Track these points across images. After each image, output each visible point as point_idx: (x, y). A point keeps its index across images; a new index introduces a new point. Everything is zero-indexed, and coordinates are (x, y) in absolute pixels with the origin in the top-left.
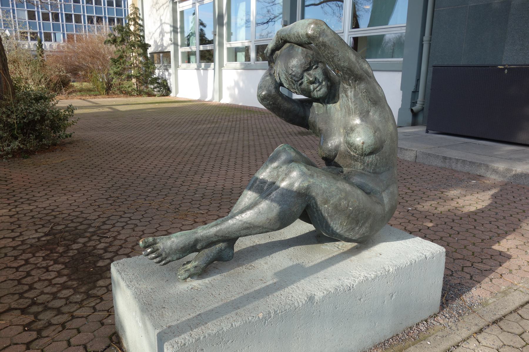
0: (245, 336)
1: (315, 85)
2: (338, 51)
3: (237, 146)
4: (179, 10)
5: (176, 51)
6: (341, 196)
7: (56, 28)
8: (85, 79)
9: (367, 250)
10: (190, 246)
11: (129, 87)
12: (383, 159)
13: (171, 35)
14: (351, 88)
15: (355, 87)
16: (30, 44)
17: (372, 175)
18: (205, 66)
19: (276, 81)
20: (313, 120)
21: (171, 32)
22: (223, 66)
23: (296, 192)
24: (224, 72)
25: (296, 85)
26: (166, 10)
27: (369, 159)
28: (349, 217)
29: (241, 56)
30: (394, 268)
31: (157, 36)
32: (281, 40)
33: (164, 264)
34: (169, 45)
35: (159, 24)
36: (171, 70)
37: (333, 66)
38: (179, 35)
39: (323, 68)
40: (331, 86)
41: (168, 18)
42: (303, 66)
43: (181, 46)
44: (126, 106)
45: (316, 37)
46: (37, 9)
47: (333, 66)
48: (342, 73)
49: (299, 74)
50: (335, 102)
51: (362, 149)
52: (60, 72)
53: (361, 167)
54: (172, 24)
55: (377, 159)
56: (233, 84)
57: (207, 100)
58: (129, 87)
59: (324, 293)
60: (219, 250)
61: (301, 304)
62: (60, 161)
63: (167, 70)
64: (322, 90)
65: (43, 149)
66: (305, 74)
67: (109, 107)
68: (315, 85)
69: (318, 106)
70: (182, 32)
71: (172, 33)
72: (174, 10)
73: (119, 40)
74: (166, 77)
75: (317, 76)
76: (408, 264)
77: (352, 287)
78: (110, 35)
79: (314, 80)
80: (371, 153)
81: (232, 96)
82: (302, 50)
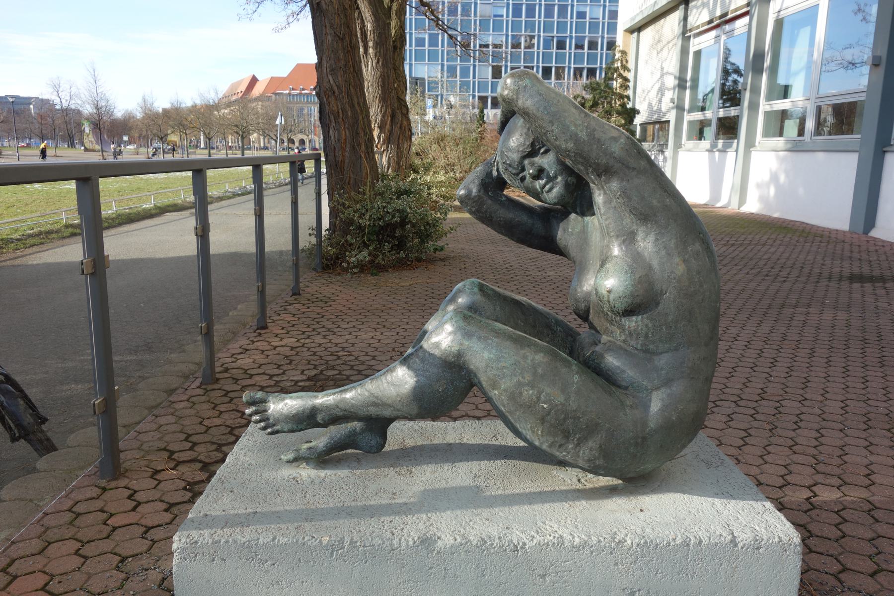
0: (294, 563)
4: (692, 49)
5: (679, 120)
6: (521, 379)
9: (628, 497)
10: (306, 414)
12: (660, 326)
13: (674, 93)
14: (599, 189)
15: (603, 188)
16: (490, 113)
17: (641, 355)
18: (723, 146)
21: (674, 88)
22: (754, 146)
23: (440, 358)
24: (755, 155)
26: (671, 52)
27: (631, 323)
28: (543, 420)
29: (791, 128)
30: (637, 540)
31: (653, 96)
33: (271, 434)
34: (669, 111)
35: (659, 76)
36: (668, 153)
38: (688, 92)
41: (672, 64)
42: (521, 149)
43: (690, 111)
46: (474, 62)
49: (516, 163)
51: (609, 302)
53: (620, 336)
54: (678, 75)
55: (647, 326)
56: (766, 177)
57: (718, 205)
59: (456, 540)
60: (350, 432)
61: (404, 544)
62: (408, 284)
64: (555, 190)
65: (402, 265)
66: (526, 162)
68: (542, 182)
70: (695, 86)
71: (677, 90)
72: (684, 51)
74: (660, 163)
76: (678, 541)
77: (522, 548)
80: (629, 312)
81: (763, 199)
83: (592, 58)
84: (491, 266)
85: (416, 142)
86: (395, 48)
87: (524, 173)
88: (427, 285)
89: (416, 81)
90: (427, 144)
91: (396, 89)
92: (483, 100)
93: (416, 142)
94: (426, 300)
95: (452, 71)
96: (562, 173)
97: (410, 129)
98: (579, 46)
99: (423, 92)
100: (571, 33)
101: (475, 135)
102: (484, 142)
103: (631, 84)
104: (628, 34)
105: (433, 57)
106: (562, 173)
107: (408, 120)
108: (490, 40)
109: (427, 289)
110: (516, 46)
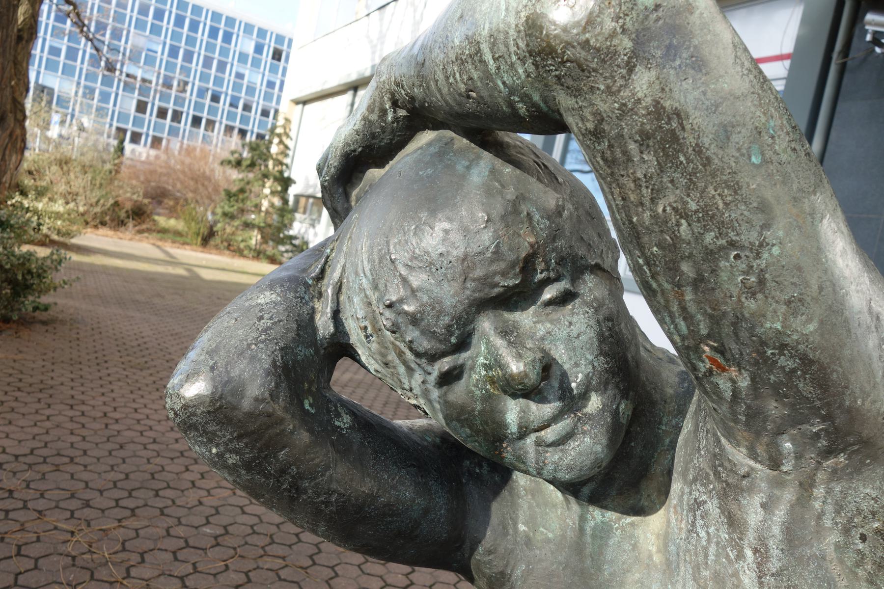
1: (533, 406)
2: (763, 207)
3: (375, 398)
7: (173, 132)
8: (172, 212)
11: (242, 241)
14: (779, 483)
15: (806, 486)
19: (306, 325)
20: (498, 565)
25: (418, 377)
32: (395, 104)
37: (688, 317)
39: (605, 311)
40: (636, 416)
42: (479, 272)
44: (217, 272)
45: (607, 55)
47: (688, 317)
48: (744, 383)
49: (446, 320)
50: (640, 511)
52: (134, 194)
58: (242, 241)
63: (313, 226)
66: (486, 324)
67: (188, 267)
69: (534, 492)
73: (245, 163)
75: (560, 354)
78: (233, 153)
79: (534, 376)
82: (493, 171)
83: (245, 120)
84: (116, 340)
85: (30, 158)
86: (20, 38)
87: (464, 356)
88: (12, 364)
89: (42, 89)
90: (45, 163)
91: (12, 87)
92: (121, 131)
93: (30, 158)
94: (6, 393)
95: (89, 92)
96: (606, 384)
97: (24, 141)
98: (234, 104)
99: (50, 102)
100: (227, 90)
101: (108, 166)
102: (119, 176)
103: (290, 153)
104: (293, 105)
105: (68, 71)
106: (606, 384)
107: (23, 129)
108: (139, 74)
109: (11, 371)
110: (168, 85)
